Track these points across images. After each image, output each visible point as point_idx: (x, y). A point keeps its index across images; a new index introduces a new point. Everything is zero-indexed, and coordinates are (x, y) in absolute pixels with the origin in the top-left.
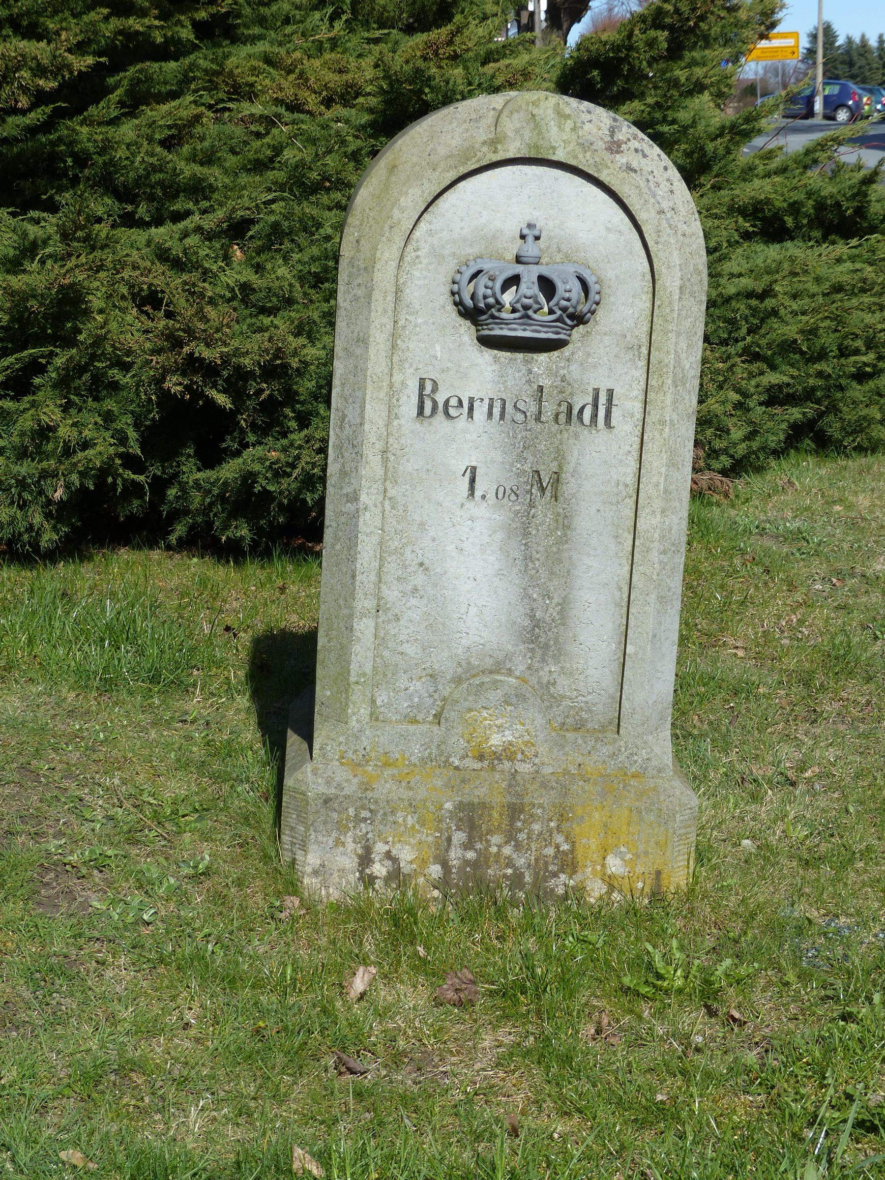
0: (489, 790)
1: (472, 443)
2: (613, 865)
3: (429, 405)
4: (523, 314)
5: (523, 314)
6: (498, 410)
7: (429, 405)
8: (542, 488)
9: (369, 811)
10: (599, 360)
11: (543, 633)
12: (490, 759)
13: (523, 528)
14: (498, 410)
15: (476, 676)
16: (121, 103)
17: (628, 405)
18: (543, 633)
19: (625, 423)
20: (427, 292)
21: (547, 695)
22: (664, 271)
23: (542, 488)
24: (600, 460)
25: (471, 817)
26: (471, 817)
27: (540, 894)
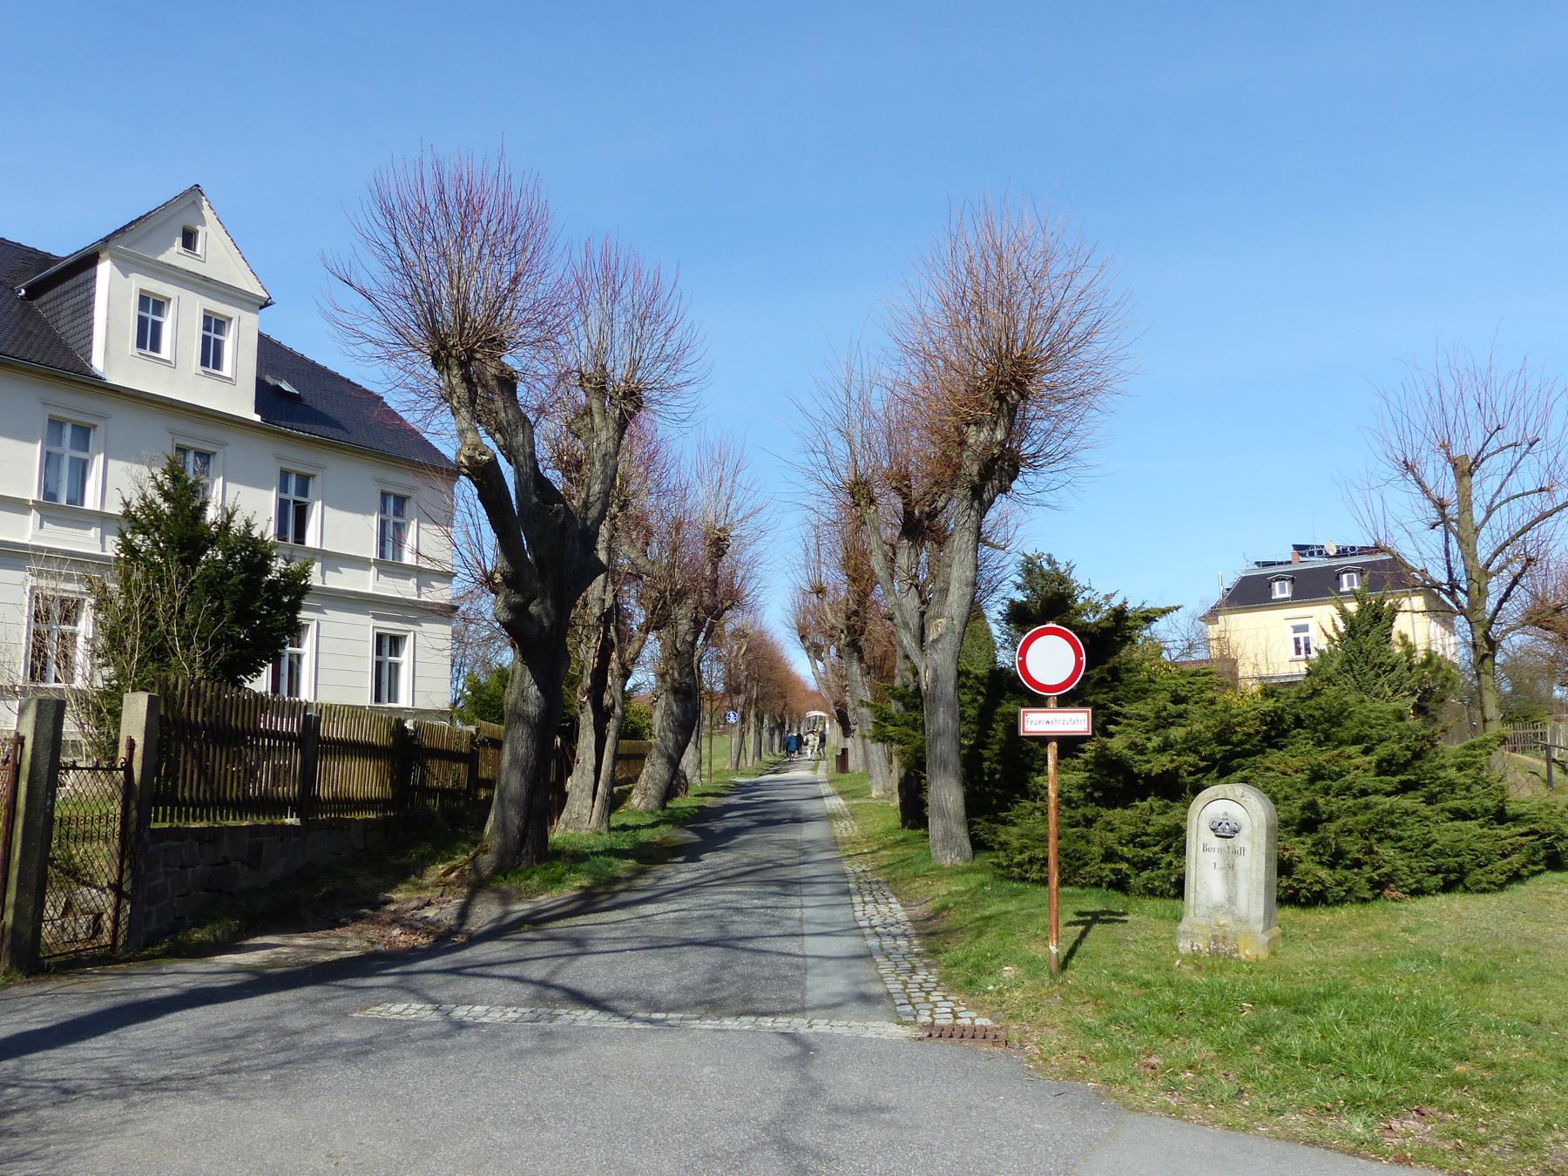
0: (1219, 933)
1: (1215, 857)
2: (1247, 953)
3: (1205, 849)
4: (1225, 831)
5: (1225, 831)
6: (1220, 850)
7: (1205, 849)
8: (1230, 867)
9: (1193, 935)
10: (1240, 841)
11: (1232, 899)
12: (1221, 926)
13: (1226, 876)
14: (1220, 850)
15: (1217, 908)
16: (153, 501)
17: (1248, 851)
18: (1232, 899)
19: (994, 611)
20: (1204, 825)
21: (1233, 913)
22: (1481, 905)
23: (1230, 867)
24: (1243, 863)
25: (1215, 938)
26: (1215, 938)
27: (1231, 957)
